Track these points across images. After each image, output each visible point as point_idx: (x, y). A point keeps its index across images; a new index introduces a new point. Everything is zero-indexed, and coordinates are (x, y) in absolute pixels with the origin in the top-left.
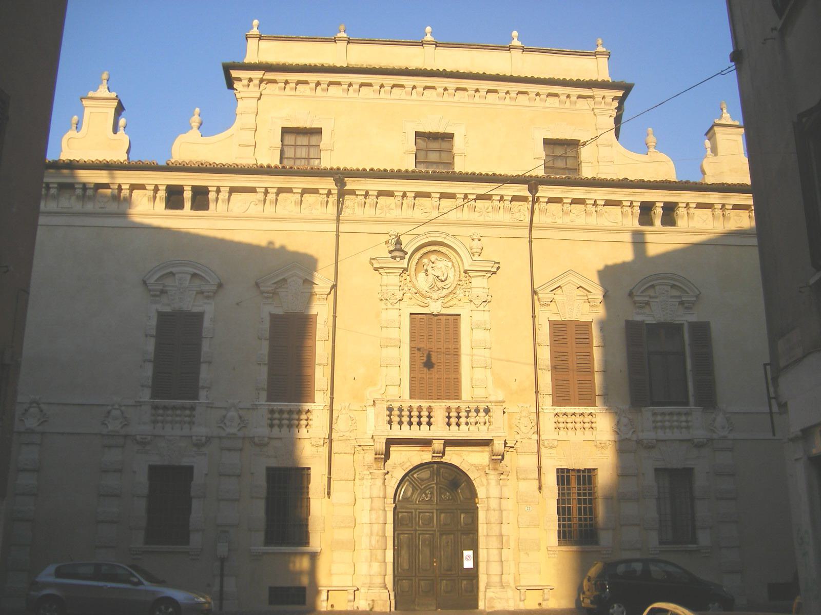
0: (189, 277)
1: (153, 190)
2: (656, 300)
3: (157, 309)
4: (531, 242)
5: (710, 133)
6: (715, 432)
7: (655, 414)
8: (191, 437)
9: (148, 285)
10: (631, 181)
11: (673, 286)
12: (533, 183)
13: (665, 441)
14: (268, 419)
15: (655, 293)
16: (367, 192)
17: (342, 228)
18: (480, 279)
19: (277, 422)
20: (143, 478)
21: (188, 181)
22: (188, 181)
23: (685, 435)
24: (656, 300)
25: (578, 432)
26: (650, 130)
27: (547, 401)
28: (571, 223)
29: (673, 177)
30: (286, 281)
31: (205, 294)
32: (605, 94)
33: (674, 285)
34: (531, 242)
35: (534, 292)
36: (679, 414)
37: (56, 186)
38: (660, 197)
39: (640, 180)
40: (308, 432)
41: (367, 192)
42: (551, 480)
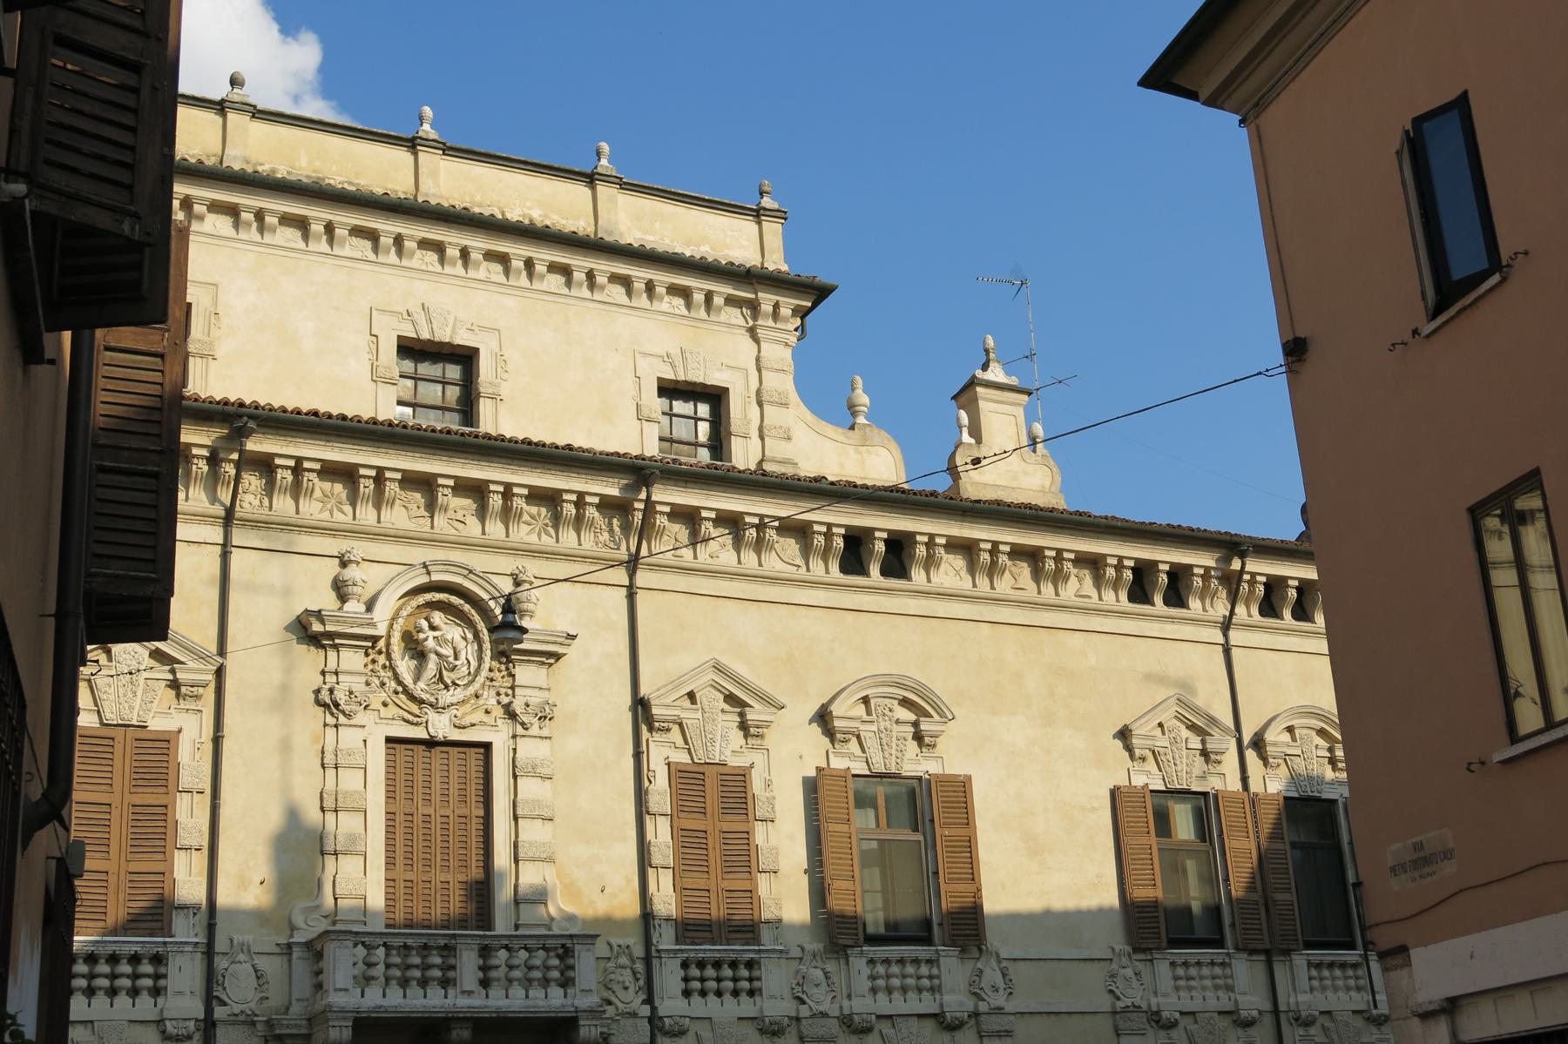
3: (752, 766)
4: (631, 596)
5: (966, 394)
6: (803, 1002)
7: (871, 962)
9: (837, 723)
10: (832, 483)
11: (905, 702)
12: (638, 472)
15: (417, 679)
17: (238, 537)
18: (533, 668)
19: (881, 983)
23: (928, 1004)
25: (727, 997)
26: (859, 381)
28: (710, 561)
29: (1057, 501)
34: (631, 596)
35: (641, 707)
36: (916, 962)
38: (883, 522)
39: (849, 483)
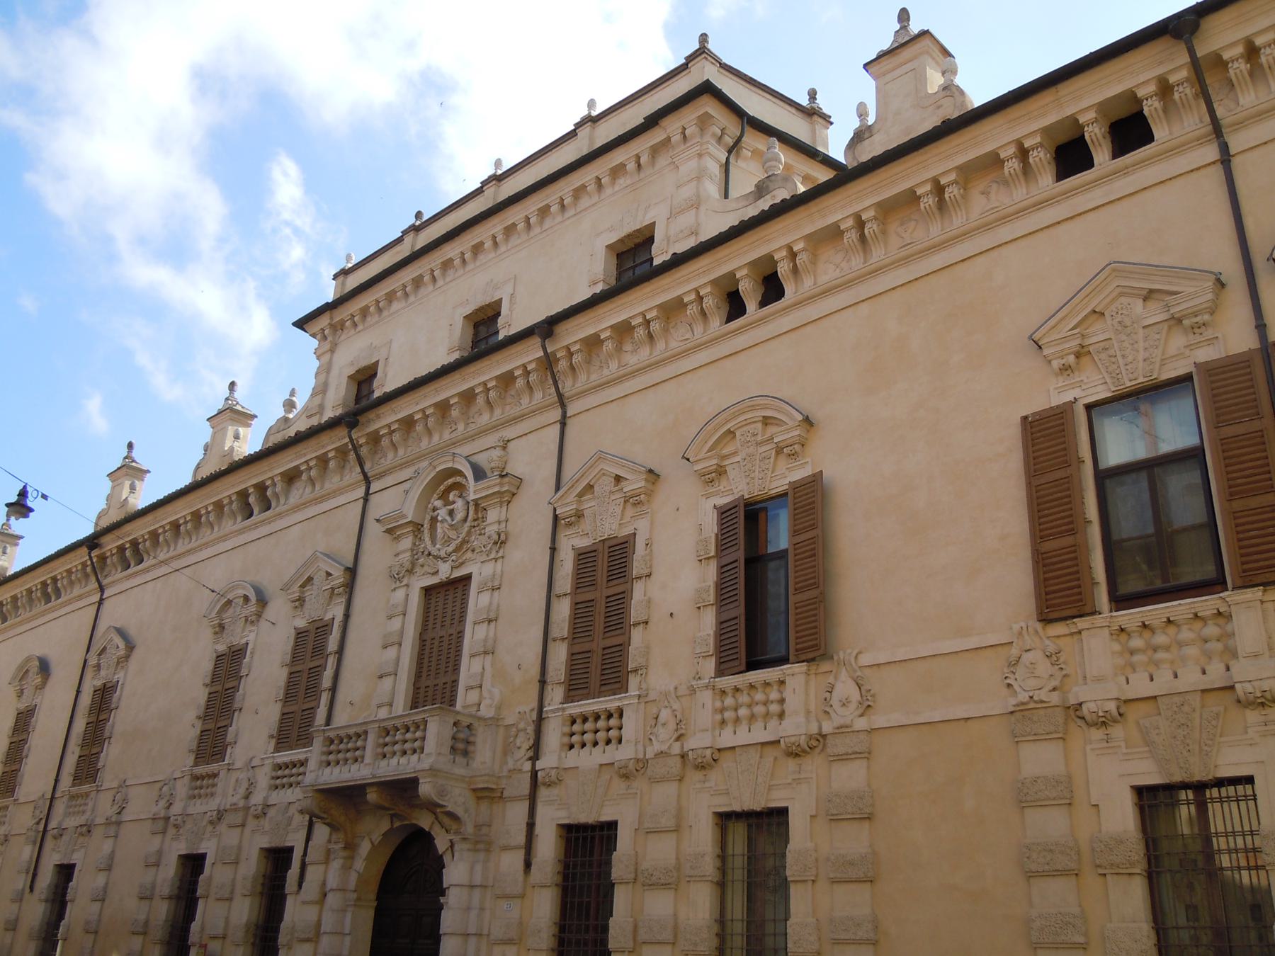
0: (759, 425)
1: (1156, 95)
2: (737, 459)
8: (1232, 688)
13: (733, 748)
14: (564, 734)
16: (790, 248)
17: (1236, 142)
20: (703, 837)
21: (737, 261)
22: (737, 261)
24: (737, 459)
27: (555, 695)
30: (733, 433)
31: (1186, 322)
32: (683, 122)
33: (1151, 291)
37: (1038, 139)
40: (1176, 676)
41: (790, 248)
42: (548, 847)
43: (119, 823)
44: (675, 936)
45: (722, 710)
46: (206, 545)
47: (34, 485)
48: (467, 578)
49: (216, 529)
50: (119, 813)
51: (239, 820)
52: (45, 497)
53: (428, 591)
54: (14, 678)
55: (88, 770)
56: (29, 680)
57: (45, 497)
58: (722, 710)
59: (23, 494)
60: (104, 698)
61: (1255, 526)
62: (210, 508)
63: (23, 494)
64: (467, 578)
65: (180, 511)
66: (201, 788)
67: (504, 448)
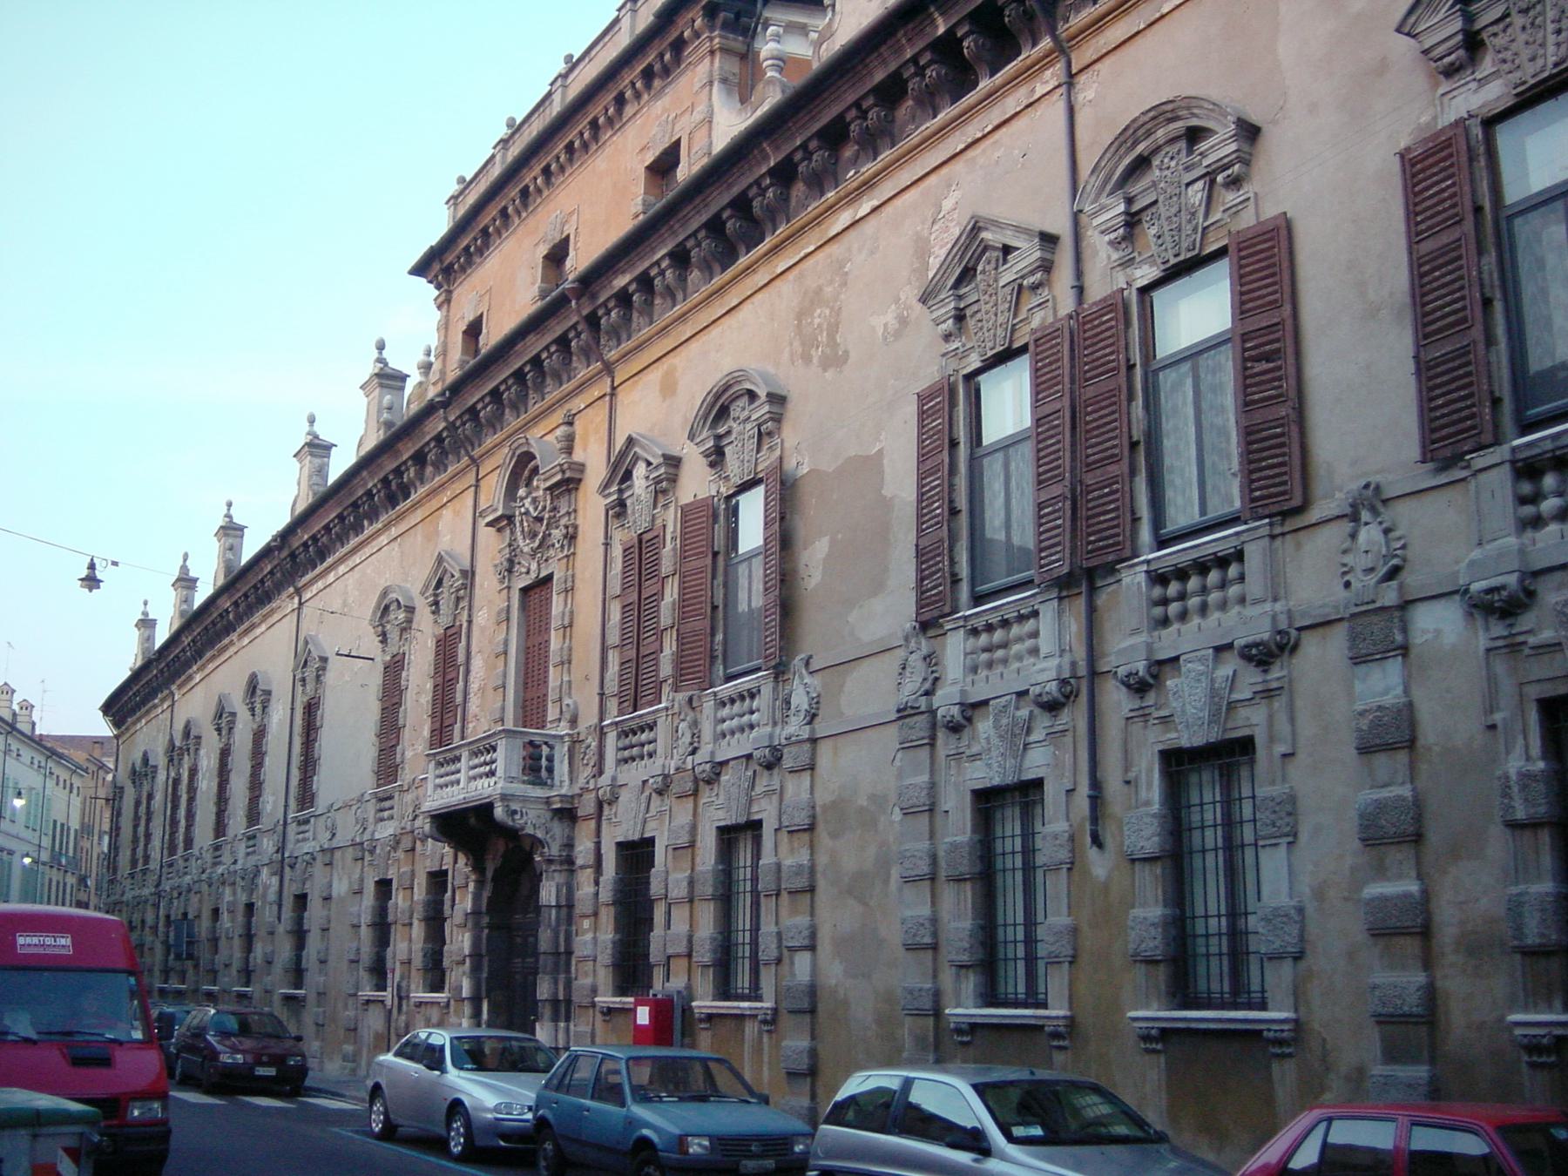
27: (613, 705)
43: (814, 741)
44: (935, 934)
45: (1165, 602)
46: (639, 347)
47: (102, 553)
48: (550, 578)
49: (680, 296)
50: (927, 693)
51: (805, 759)
52: (115, 564)
53: (525, 591)
54: (426, 587)
55: (306, 797)
56: (392, 616)
57: (115, 564)
58: (1165, 602)
59: (92, 566)
60: (311, 709)
61: (1273, 452)
62: (553, 349)
63: (92, 566)
64: (550, 578)
65: (535, 345)
66: (1005, 645)
67: (571, 424)
